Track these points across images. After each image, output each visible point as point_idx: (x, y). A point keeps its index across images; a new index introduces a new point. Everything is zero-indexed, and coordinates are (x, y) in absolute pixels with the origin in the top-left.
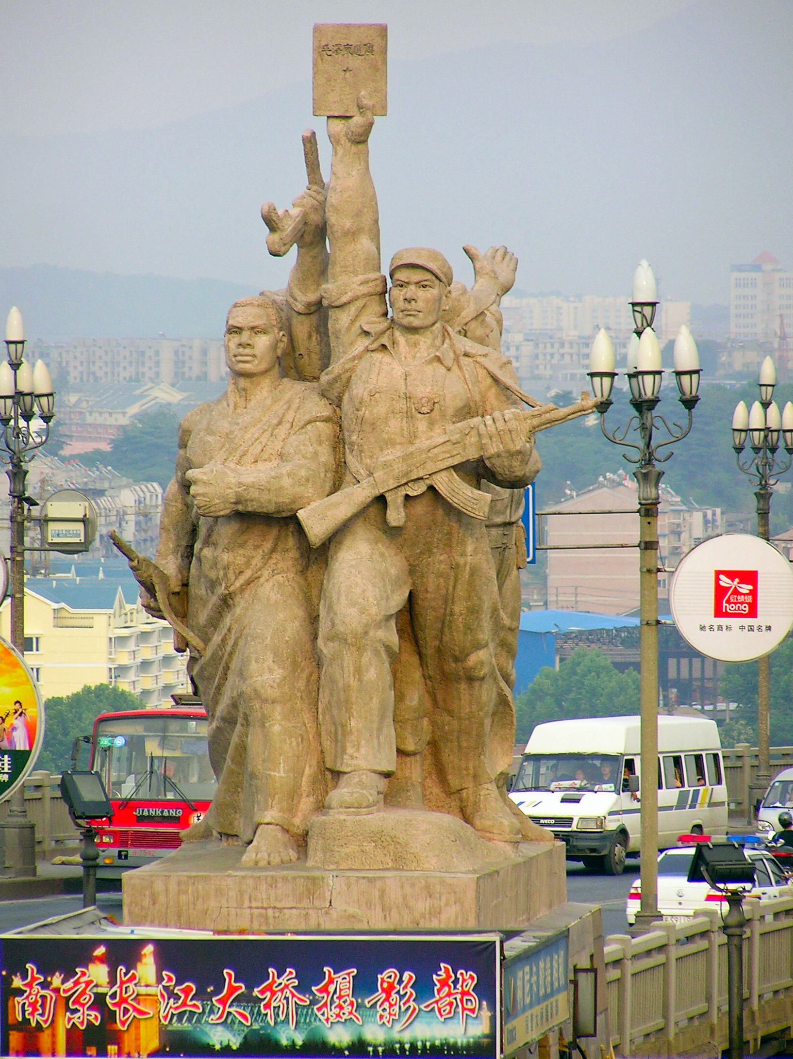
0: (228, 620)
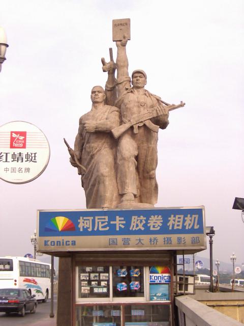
0: (93, 161)
